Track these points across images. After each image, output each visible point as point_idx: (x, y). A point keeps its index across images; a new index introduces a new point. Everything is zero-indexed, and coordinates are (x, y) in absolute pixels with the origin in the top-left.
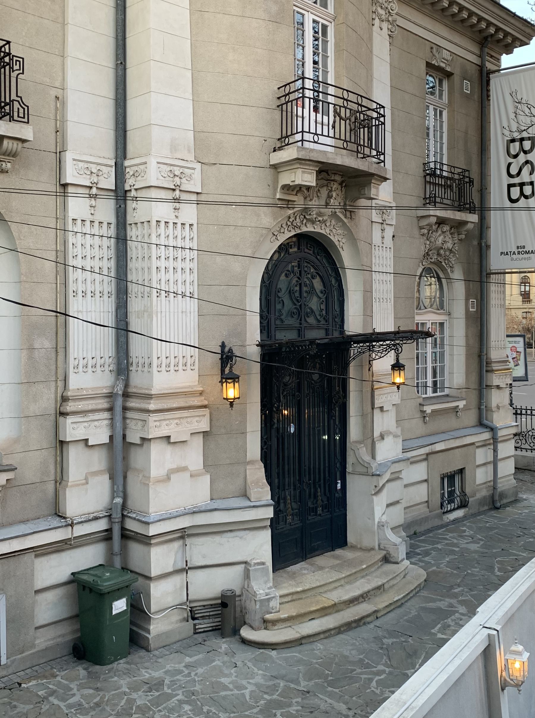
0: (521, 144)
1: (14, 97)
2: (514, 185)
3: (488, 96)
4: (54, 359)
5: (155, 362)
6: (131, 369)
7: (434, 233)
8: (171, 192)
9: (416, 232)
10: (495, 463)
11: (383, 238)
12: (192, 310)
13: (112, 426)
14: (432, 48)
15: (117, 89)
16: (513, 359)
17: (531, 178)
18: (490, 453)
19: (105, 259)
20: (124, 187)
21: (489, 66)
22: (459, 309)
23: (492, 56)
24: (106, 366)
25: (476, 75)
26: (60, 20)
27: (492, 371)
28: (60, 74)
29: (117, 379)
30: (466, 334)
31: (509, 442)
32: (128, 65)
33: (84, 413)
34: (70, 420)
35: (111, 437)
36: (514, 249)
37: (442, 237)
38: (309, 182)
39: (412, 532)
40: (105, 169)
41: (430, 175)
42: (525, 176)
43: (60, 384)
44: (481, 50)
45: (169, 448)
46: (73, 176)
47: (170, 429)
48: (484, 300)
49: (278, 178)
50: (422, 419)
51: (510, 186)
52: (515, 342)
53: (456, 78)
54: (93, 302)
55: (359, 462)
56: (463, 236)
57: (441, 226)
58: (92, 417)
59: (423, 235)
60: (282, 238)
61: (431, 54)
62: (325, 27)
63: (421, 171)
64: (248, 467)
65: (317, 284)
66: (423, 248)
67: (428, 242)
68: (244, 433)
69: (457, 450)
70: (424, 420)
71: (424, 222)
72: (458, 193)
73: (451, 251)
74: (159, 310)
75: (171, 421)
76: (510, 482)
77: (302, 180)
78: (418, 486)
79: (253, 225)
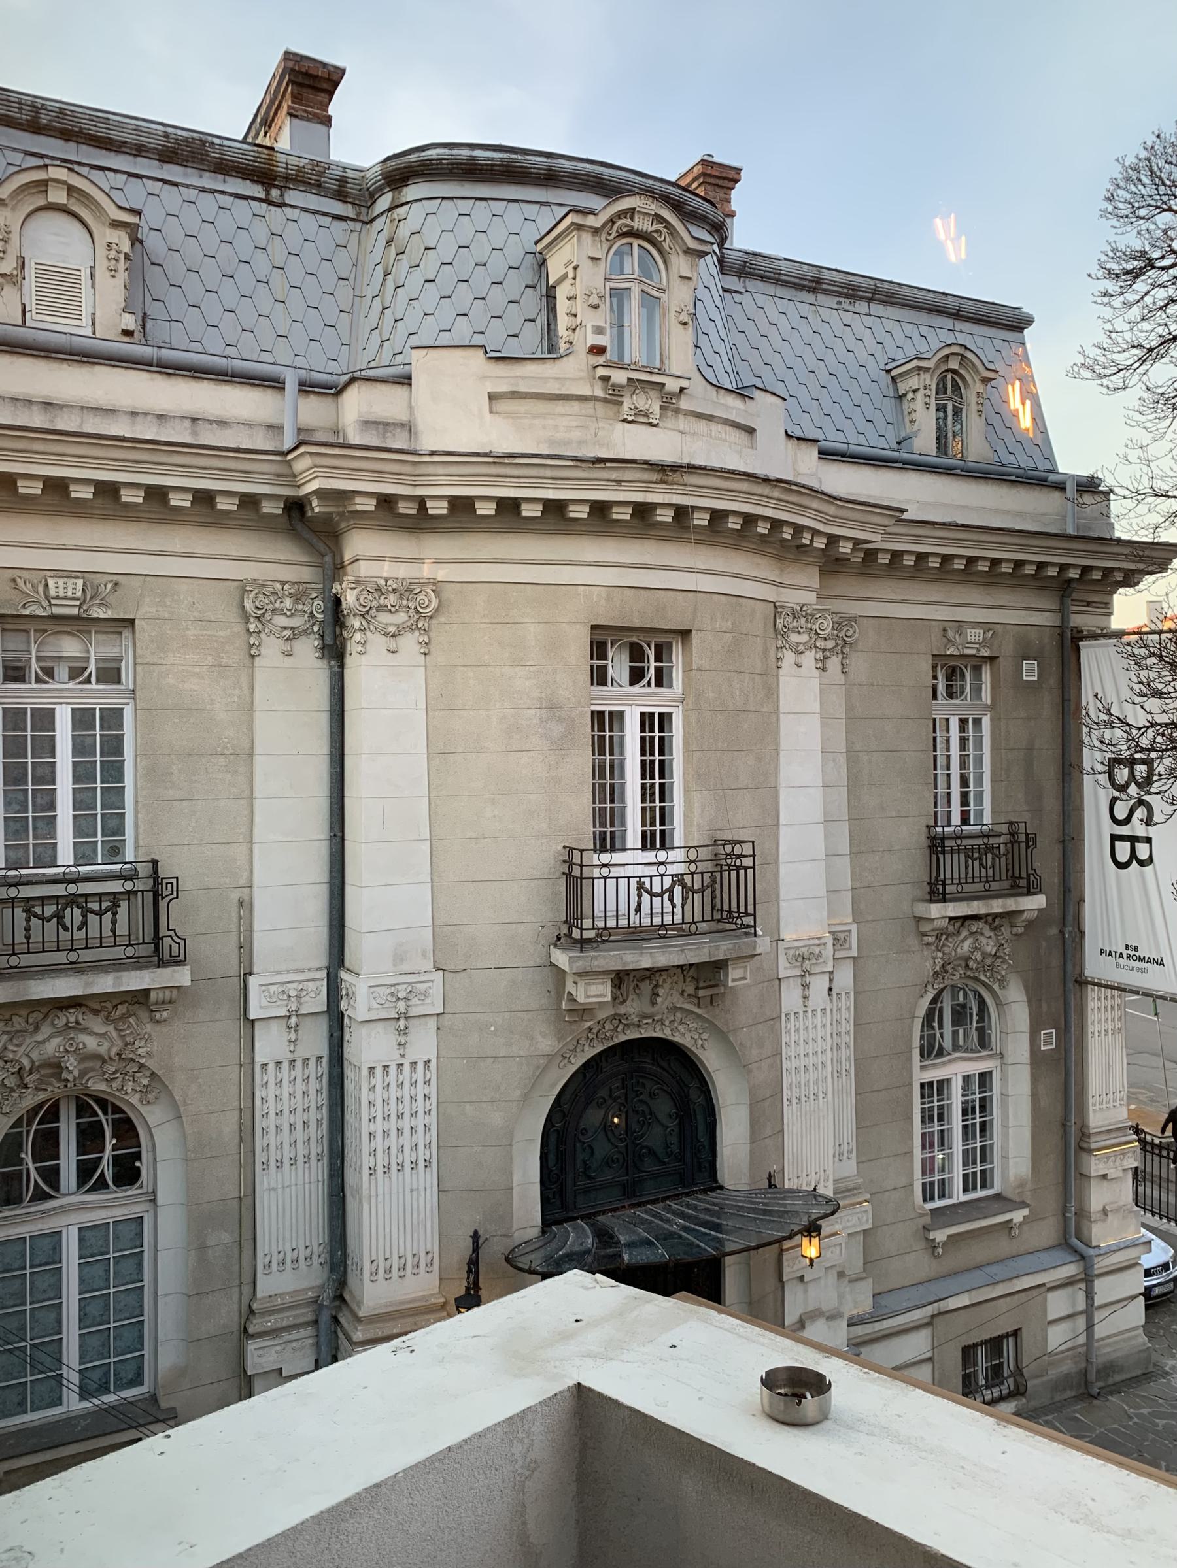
4: (237, 1256)
8: (393, 1022)
9: (913, 942)
10: (1089, 1312)
11: (805, 997)
12: (428, 1185)
14: (945, 630)
17: (1147, 831)
18: (1081, 1296)
20: (338, 1006)
21: (1081, 620)
22: (1018, 1048)
24: (315, 1257)
26: (247, 793)
27: (1090, 1151)
30: (1032, 1089)
33: (275, 1332)
38: (598, 996)
40: (311, 986)
43: (247, 1290)
44: (1062, 603)
46: (261, 1007)
50: (930, 1250)
51: (1114, 838)
53: (1004, 664)
54: (293, 1173)
56: (1020, 930)
57: (967, 923)
58: (286, 1337)
59: (928, 944)
60: (578, 1062)
61: (945, 640)
66: (928, 964)
69: (1002, 1300)
71: (926, 927)
74: (373, 1193)
76: (1133, 1342)
77: (587, 996)
79: (522, 1053)
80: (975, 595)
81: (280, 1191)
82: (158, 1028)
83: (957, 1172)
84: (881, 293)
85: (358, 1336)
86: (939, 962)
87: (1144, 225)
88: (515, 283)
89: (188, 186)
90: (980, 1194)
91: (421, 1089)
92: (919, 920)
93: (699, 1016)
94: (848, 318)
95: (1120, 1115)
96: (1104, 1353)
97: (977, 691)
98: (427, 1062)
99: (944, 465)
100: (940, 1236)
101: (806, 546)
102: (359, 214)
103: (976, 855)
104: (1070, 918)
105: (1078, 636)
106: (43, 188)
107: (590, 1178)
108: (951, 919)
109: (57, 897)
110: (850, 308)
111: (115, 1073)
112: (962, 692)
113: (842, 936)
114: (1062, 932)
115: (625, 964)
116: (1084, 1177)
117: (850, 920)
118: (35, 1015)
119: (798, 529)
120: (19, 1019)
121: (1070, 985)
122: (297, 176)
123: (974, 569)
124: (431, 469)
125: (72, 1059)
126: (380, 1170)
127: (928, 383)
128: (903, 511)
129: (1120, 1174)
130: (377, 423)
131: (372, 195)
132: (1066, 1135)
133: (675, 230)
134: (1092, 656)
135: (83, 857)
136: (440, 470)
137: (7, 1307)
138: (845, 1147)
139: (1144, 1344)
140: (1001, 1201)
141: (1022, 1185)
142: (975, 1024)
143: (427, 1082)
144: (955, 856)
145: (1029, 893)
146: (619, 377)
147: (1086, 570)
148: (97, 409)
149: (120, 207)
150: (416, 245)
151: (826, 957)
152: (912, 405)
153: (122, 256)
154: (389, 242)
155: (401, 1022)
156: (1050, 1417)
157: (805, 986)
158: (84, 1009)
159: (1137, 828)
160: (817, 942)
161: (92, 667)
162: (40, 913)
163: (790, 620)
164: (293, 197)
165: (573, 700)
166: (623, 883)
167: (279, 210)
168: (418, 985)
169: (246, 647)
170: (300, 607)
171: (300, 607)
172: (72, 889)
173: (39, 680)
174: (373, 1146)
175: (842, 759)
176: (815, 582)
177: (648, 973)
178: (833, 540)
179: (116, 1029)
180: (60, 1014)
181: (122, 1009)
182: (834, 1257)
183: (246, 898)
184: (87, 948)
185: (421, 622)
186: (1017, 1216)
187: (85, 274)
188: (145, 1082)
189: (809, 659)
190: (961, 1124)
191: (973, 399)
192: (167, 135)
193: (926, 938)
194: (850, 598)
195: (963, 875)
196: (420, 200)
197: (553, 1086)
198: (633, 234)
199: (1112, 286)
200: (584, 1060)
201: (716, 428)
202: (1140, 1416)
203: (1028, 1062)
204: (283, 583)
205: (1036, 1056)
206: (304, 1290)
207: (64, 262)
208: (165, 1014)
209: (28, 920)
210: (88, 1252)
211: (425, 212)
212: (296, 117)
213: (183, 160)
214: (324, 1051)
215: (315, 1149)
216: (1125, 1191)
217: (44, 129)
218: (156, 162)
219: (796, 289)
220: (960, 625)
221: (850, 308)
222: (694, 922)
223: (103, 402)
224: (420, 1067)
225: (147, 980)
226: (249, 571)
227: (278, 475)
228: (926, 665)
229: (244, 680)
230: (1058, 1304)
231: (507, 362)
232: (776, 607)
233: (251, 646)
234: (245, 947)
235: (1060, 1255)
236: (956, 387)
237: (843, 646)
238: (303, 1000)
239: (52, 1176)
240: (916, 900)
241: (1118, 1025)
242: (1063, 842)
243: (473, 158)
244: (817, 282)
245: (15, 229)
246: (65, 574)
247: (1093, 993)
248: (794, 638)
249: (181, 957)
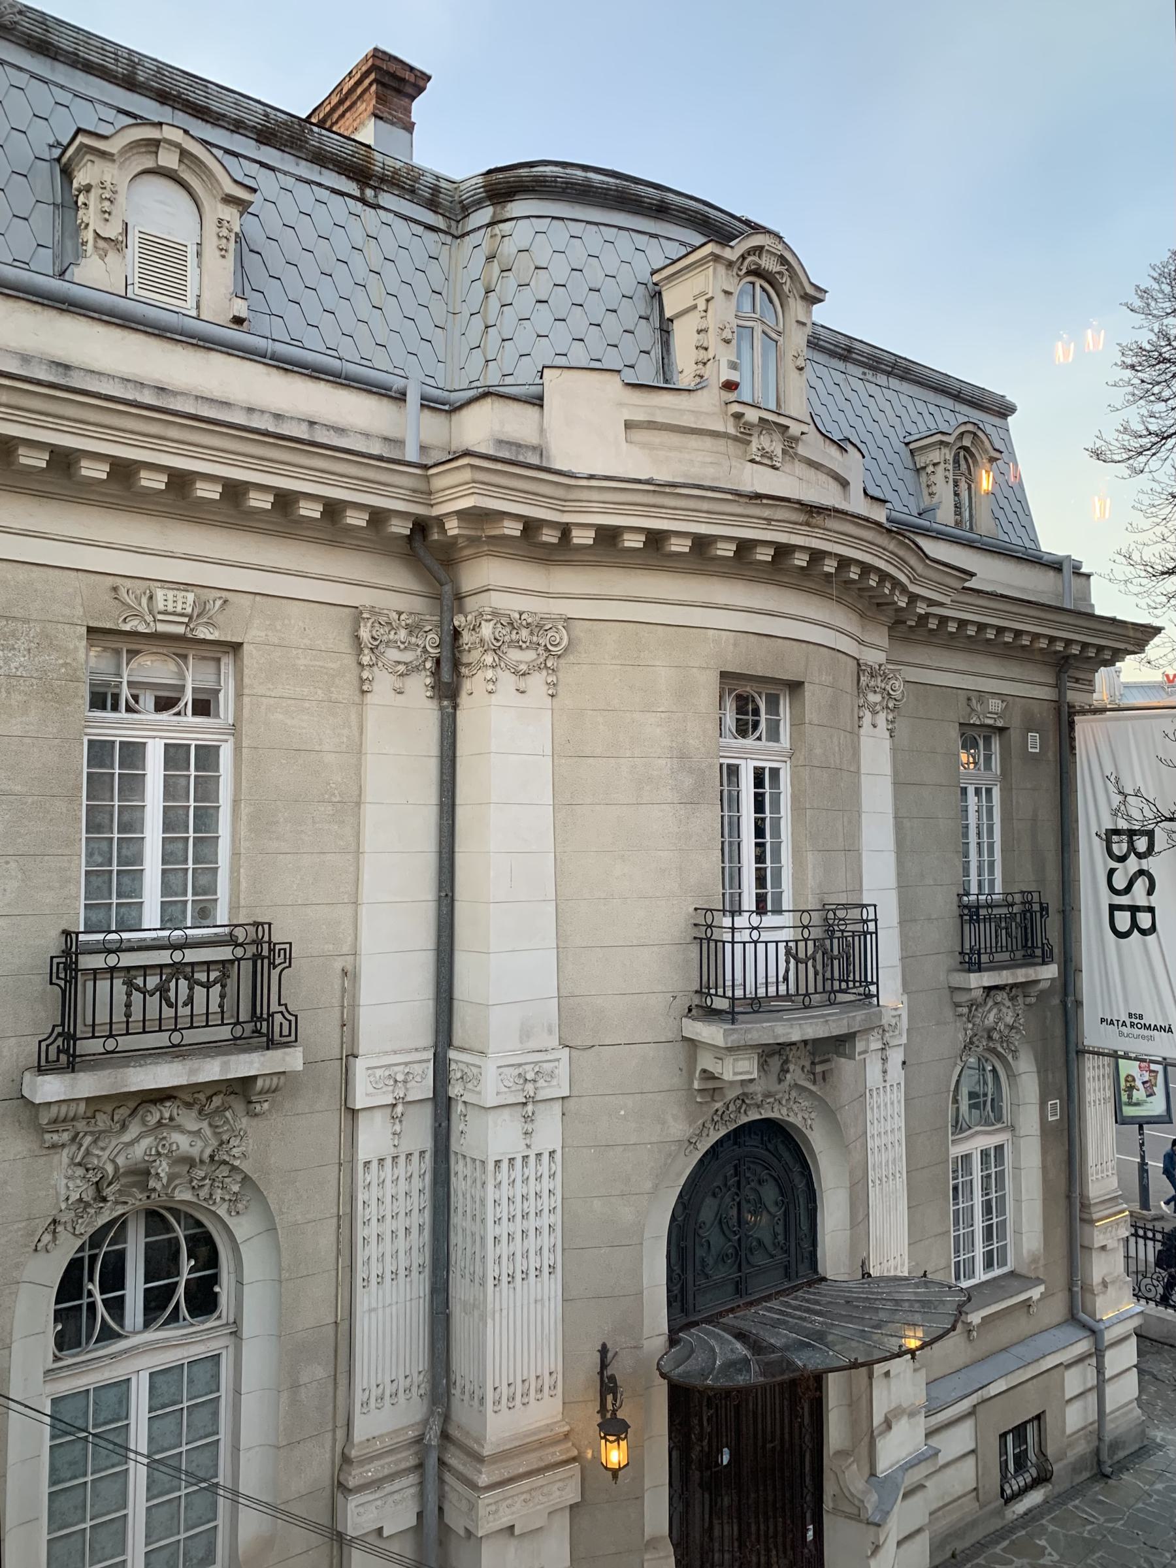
1: (274, 1007)
2: (1121, 908)
3: (1073, 748)
4: (331, 1394)
5: (490, 1397)
6: (453, 1391)
7: (980, 1010)
8: (519, 1108)
9: (948, 1013)
11: (885, 1072)
13: (422, 1495)
14: (969, 699)
15: (439, 937)
16: (1144, 1083)
17: (1149, 901)
19: (415, 1212)
20: (446, 1092)
22: (1029, 1121)
23: (1077, 680)
24: (414, 1389)
25: (1049, 718)
28: (351, 931)
29: (432, 1413)
31: (1127, 1343)
32: (457, 896)
34: (354, 1501)
35: (420, 1515)
36: (1124, 1017)
37: (995, 1011)
39: (949, 1554)
40: (417, 1069)
41: (970, 914)
42: (1138, 895)
43: (341, 1434)
44: (1058, 678)
45: (512, 1545)
46: (367, 1095)
47: (513, 1513)
48: (1073, 1102)
49: (695, 1054)
51: (1113, 908)
53: (1014, 735)
55: (843, 1494)
56: (1033, 1000)
57: (992, 993)
58: (388, 1488)
59: (961, 1015)
60: (704, 1146)
61: (969, 709)
62: (775, 773)
63: (955, 907)
64: (647, 1557)
65: (770, 1193)
66: (961, 1036)
67: (970, 1026)
68: (640, 1498)
69: (1030, 1383)
70: (969, 1337)
71: (962, 998)
72: (1020, 937)
73: (1012, 1028)
74: (497, 1308)
75: (516, 1498)
76: (1130, 1416)
77: (735, 1074)
78: (959, 1465)
79: (654, 1139)
80: (991, 666)
81: (380, 1311)
82: (254, 1122)
85: (483, 1480)
88: (629, 313)
89: (285, 173)
91: (546, 1184)
92: (953, 990)
93: (811, 1092)
96: (1112, 1428)
97: (774, 735)
98: (552, 1153)
102: (449, 227)
106: (154, 149)
107: (707, 1277)
109: (161, 966)
110: (873, 379)
111: (204, 1179)
115: (776, 1037)
116: (1087, 1249)
118: (121, 1111)
120: (104, 1117)
122: (393, 178)
124: (585, 495)
125: (164, 1164)
126: (505, 1279)
130: (508, 443)
131: (465, 208)
132: (1070, 1205)
133: (796, 274)
135: (170, 920)
136: (595, 496)
137: (64, 1481)
139: (1139, 1418)
141: (1035, 1260)
143: (552, 1176)
145: (1044, 963)
146: (752, 415)
148: (212, 400)
149: (236, 181)
150: (523, 265)
151: (901, 1030)
153: (233, 236)
154: (491, 258)
155: (526, 1107)
156: (1077, 1502)
157: (884, 1060)
158: (178, 1103)
159: (1138, 895)
161: (188, 697)
162: (142, 985)
164: (386, 199)
165: (703, 750)
166: (771, 946)
167: (372, 211)
168: (545, 1065)
169: (356, 683)
170: (413, 640)
171: (413, 640)
172: (177, 956)
173: (129, 709)
174: (498, 1252)
176: (884, 642)
177: (778, 1047)
179: (210, 1125)
180: (153, 1109)
181: (217, 1101)
183: (349, 968)
184: (128, 1034)
185: (551, 658)
186: (1036, 1293)
187: (192, 250)
188: (236, 1188)
189: (881, 718)
192: (267, 115)
195: (994, 945)
196: (528, 217)
197: (679, 1175)
198: (757, 272)
200: (709, 1145)
201: (823, 477)
202: (1158, 1492)
203: (1038, 1133)
204: (400, 614)
205: (1046, 1129)
206: (402, 1429)
207: (169, 234)
208: (266, 1106)
209: (129, 995)
210: (160, 1401)
211: (529, 227)
212: (381, 118)
213: (282, 144)
214: (428, 1144)
215: (417, 1259)
217: (140, 87)
218: (253, 142)
219: (830, 355)
222: (807, 994)
223: (217, 394)
224: (545, 1158)
225: (256, 1065)
226: (362, 598)
227: (414, 491)
229: (354, 717)
230: (1075, 1381)
231: (644, 390)
232: (859, 665)
233: (362, 681)
234: (348, 1025)
238: (409, 1085)
239: (116, 1307)
240: (951, 970)
242: (1063, 911)
243: (588, 179)
244: (849, 351)
245: (122, 188)
246: (182, 587)
247: (1090, 1062)
248: (514, 655)
249: (293, 1038)
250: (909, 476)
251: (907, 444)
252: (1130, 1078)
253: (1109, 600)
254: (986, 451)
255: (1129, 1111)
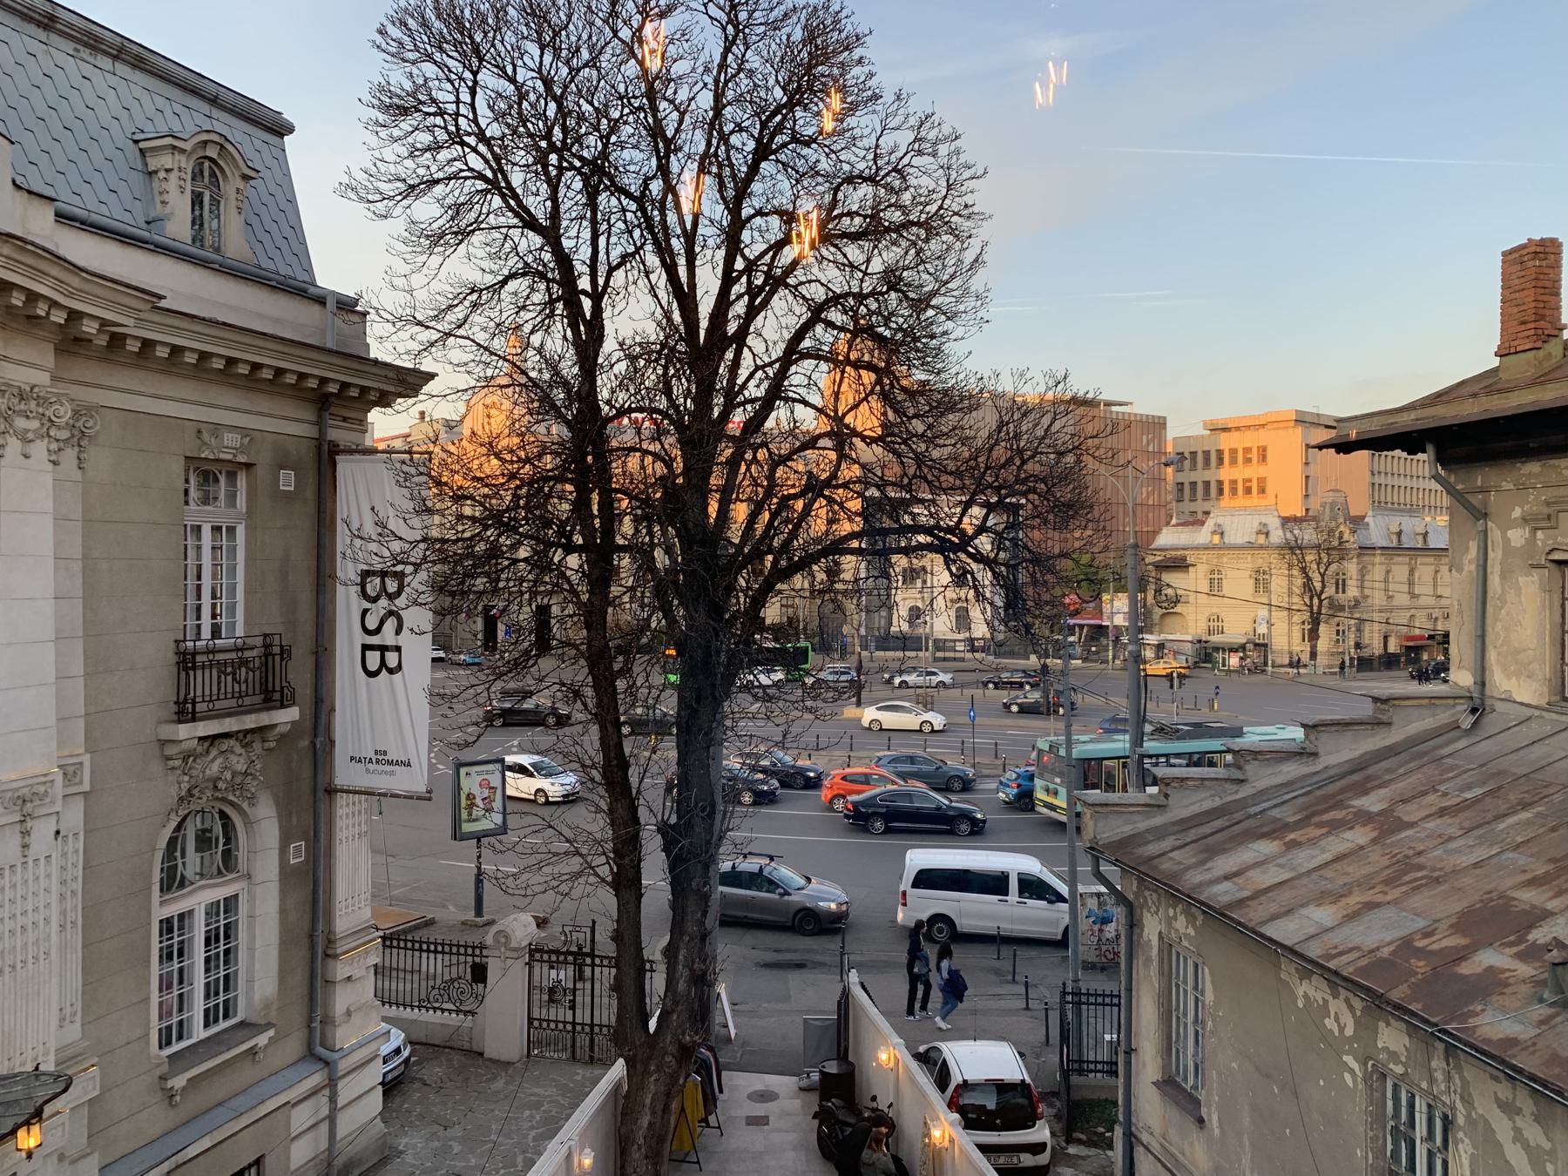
0: (383, 582)
9: (156, 767)
11: (25, 846)
21: (338, 434)
27: (335, 957)
36: (371, 755)
37: (220, 760)
44: (320, 416)
52: (488, 772)
53: (261, 471)
56: (272, 745)
59: (173, 768)
71: (171, 750)
80: (232, 397)
83: (199, 1006)
84: (128, 53)
86: (185, 786)
87: (409, 67)
90: (223, 1025)
92: (163, 743)
94: (88, 70)
95: (365, 915)
96: (344, 1154)
97: (232, 497)
99: (200, 255)
100: (179, 1082)
101: (39, 317)
103: (229, 670)
104: (322, 728)
105: (335, 450)
108: (200, 739)
110: (91, 59)
112: (216, 498)
113: (71, 769)
114: (313, 744)
116: (329, 983)
117: (82, 750)
119: (32, 297)
121: (321, 794)
123: (207, 366)
127: (183, 165)
128: (161, 297)
129: (363, 972)
132: (312, 943)
134: (346, 468)
138: (68, 1010)
140: (248, 1027)
142: (221, 847)
144: (207, 672)
145: (283, 706)
147: (345, 386)
152: (164, 185)
159: (388, 636)
160: (43, 779)
163: (16, 401)
175: (77, 567)
176: (49, 359)
178: (74, 316)
182: (58, 1140)
186: (262, 1040)
189: (40, 449)
190: (203, 955)
191: (233, 195)
193: (171, 763)
194: (86, 384)
199: (382, 118)
205: (286, 873)
216: (367, 988)
220: (216, 428)
221: (91, 59)
228: (178, 467)
230: (301, 1118)
235: (304, 1068)
236: (213, 174)
237: (79, 437)
241: (364, 828)
247: (341, 800)
248: (20, 423)
250: (136, 179)
251: (136, 142)
252: (470, 797)
253: (386, 344)
254: (237, 167)
255: (467, 827)
